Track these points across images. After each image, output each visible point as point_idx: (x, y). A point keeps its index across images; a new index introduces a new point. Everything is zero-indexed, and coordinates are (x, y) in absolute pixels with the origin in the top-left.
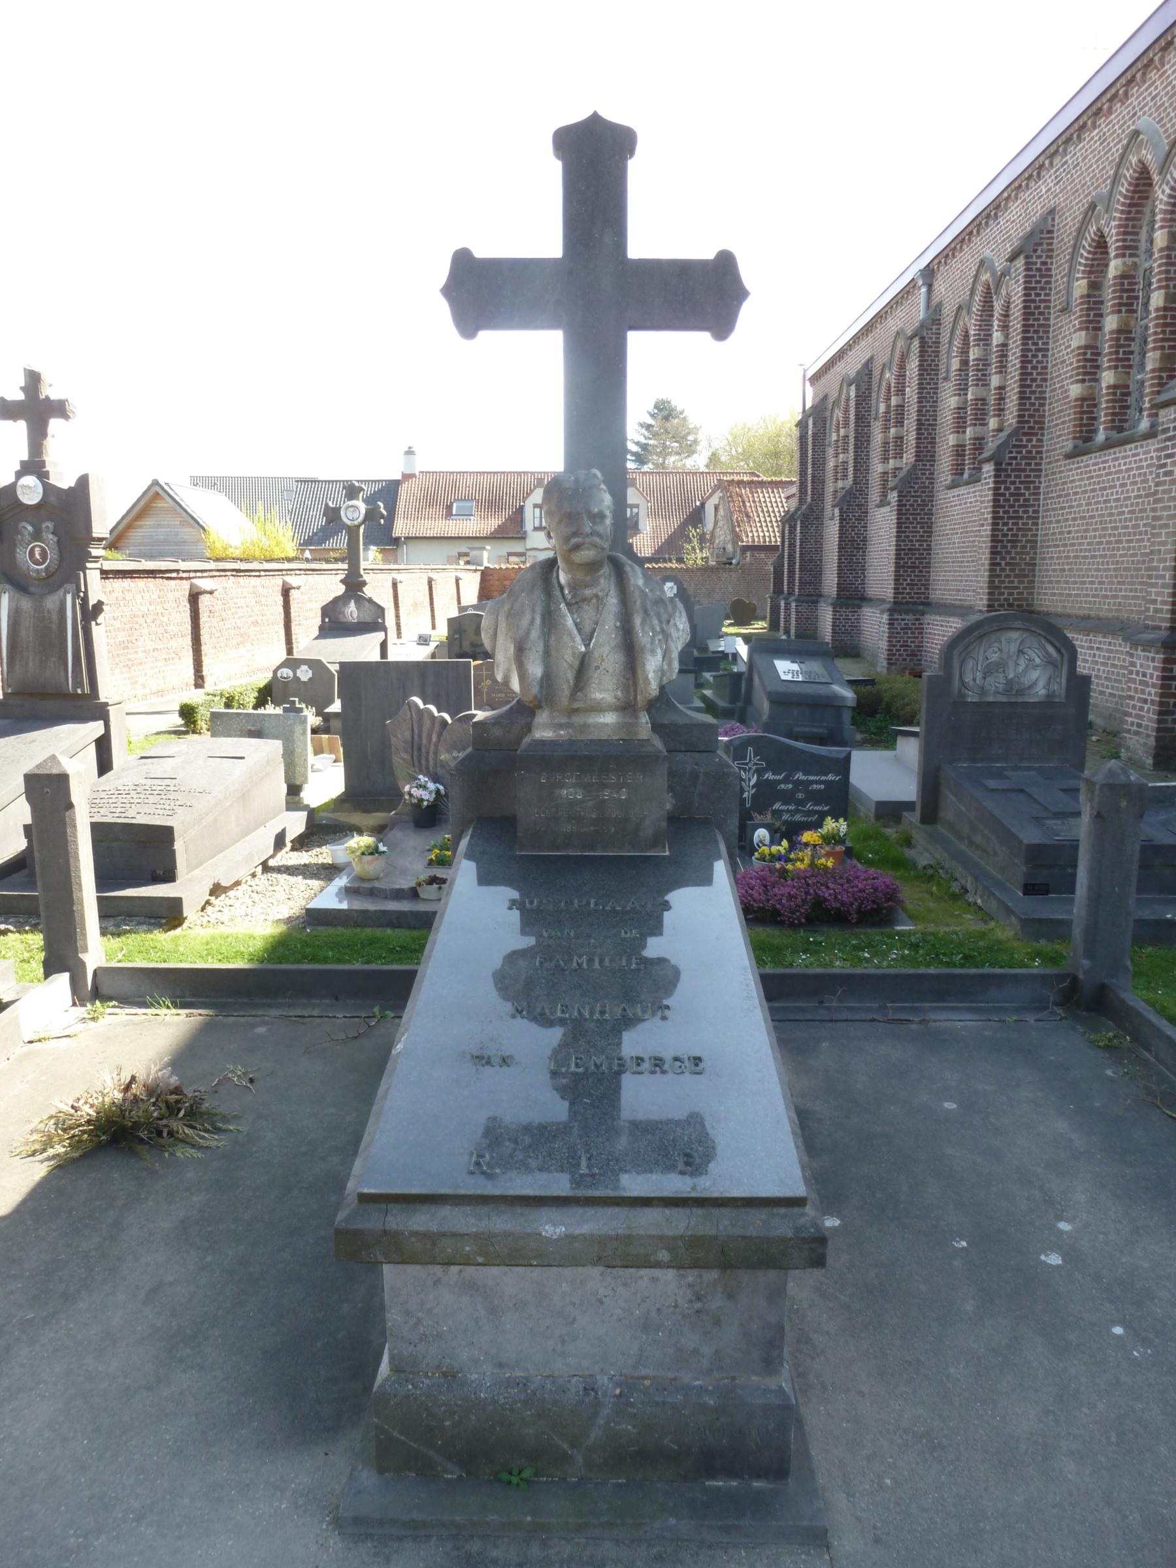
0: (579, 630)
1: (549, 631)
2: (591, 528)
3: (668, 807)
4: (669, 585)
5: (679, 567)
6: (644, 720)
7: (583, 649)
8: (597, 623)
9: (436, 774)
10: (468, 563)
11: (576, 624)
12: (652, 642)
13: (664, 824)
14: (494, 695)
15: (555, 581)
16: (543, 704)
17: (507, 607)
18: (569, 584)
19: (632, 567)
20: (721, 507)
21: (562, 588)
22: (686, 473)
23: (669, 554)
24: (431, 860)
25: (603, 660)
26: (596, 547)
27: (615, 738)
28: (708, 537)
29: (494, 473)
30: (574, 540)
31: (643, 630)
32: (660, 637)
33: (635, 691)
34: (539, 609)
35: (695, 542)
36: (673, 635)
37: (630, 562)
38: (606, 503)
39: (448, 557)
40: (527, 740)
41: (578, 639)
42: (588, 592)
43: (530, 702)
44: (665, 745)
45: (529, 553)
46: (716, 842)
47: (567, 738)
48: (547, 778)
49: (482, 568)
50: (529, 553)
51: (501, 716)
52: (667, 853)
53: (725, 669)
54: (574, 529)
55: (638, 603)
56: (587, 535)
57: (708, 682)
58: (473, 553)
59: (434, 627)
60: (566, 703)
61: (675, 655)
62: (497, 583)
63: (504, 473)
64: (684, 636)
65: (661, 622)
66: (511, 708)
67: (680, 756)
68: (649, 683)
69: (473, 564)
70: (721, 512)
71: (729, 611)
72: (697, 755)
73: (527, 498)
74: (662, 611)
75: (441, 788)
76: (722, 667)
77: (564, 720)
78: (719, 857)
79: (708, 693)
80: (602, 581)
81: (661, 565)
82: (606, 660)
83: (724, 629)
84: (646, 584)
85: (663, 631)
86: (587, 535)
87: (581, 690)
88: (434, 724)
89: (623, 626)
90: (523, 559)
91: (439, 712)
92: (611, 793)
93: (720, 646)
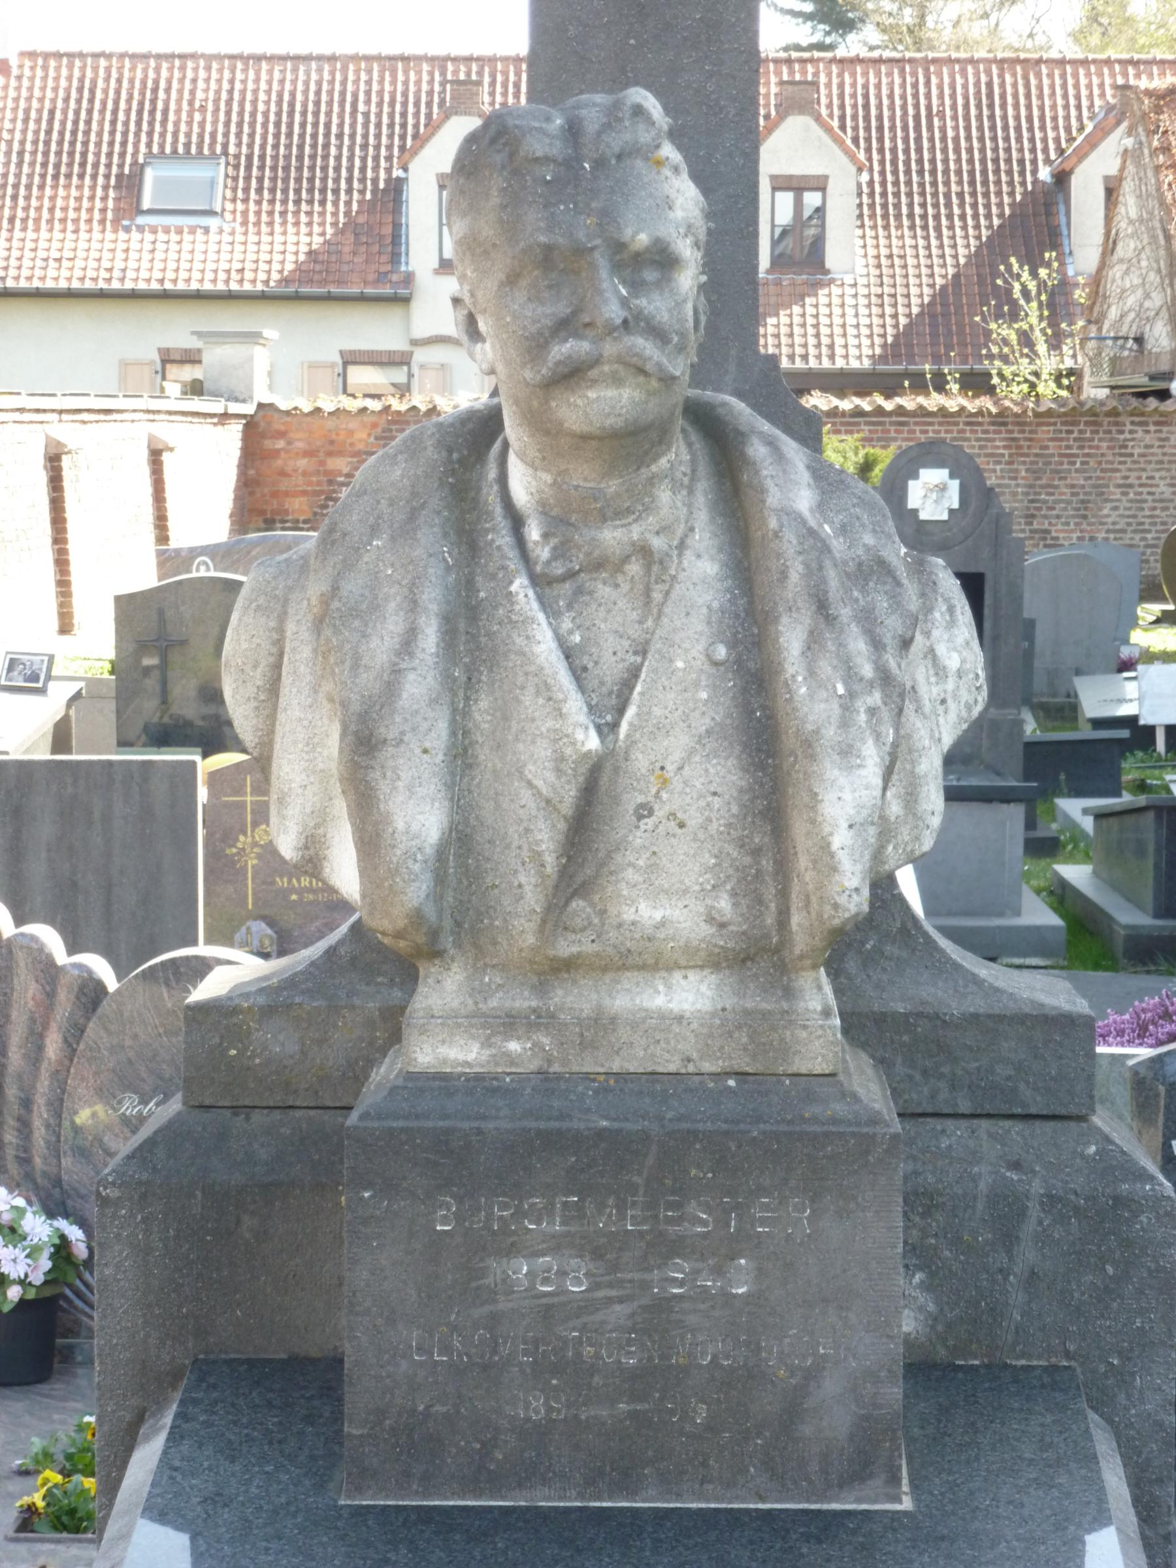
0: (579, 674)
1: (470, 682)
2: (624, 303)
3: (909, 1324)
4: (932, 476)
5: (972, 406)
6: (815, 1005)
7: (593, 742)
8: (643, 652)
9: (58, 1182)
10: (196, 389)
11: (568, 654)
12: (845, 723)
13: (894, 1393)
14: (282, 882)
15: (491, 496)
16: (447, 942)
17: (316, 588)
18: (544, 509)
19: (771, 443)
20: (1128, 187)
21: (517, 522)
22: (1001, 62)
23: (937, 359)
24: (31, 1509)
25: (665, 782)
26: (641, 371)
27: (707, 1067)
28: (1080, 295)
29: (297, 58)
30: (565, 349)
31: (811, 673)
32: (876, 698)
33: (784, 894)
34: (432, 597)
35: (1033, 315)
36: (923, 690)
37: (766, 426)
38: (678, 214)
39: (125, 365)
40: (384, 1073)
41: (575, 705)
42: (612, 537)
43: (399, 935)
44: (896, 1093)
45: (421, 356)
46: (1091, 1460)
47: (533, 1066)
48: (459, 1218)
49: (249, 409)
50: (421, 356)
51: (291, 983)
52: (906, 1504)
53: (1141, 787)
54: (562, 309)
55: (795, 575)
56: (610, 330)
57: (1077, 834)
58: (216, 356)
59: (65, 627)
60: (531, 940)
61: (930, 766)
62: (302, 463)
63: (332, 59)
64: (965, 696)
65: (877, 645)
66: (331, 952)
67: (955, 1134)
68: (835, 869)
69: (216, 394)
70: (1129, 206)
71: (1156, 568)
72: (1016, 1127)
73: (415, 152)
74: (882, 603)
75: (75, 1234)
76: (1127, 777)
77: (523, 1001)
78: (1101, 1519)
79: (1076, 873)
80: (664, 495)
81: (909, 402)
82: (677, 783)
83: (1140, 638)
84: (821, 507)
85: (885, 679)
86: (610, 330)
87: (583, 890)
88: (51, 995)
89: (739, 662)
90: (399, 376)
91: (72, 949)
92: (696, 1272)
93: (1122, 701)
